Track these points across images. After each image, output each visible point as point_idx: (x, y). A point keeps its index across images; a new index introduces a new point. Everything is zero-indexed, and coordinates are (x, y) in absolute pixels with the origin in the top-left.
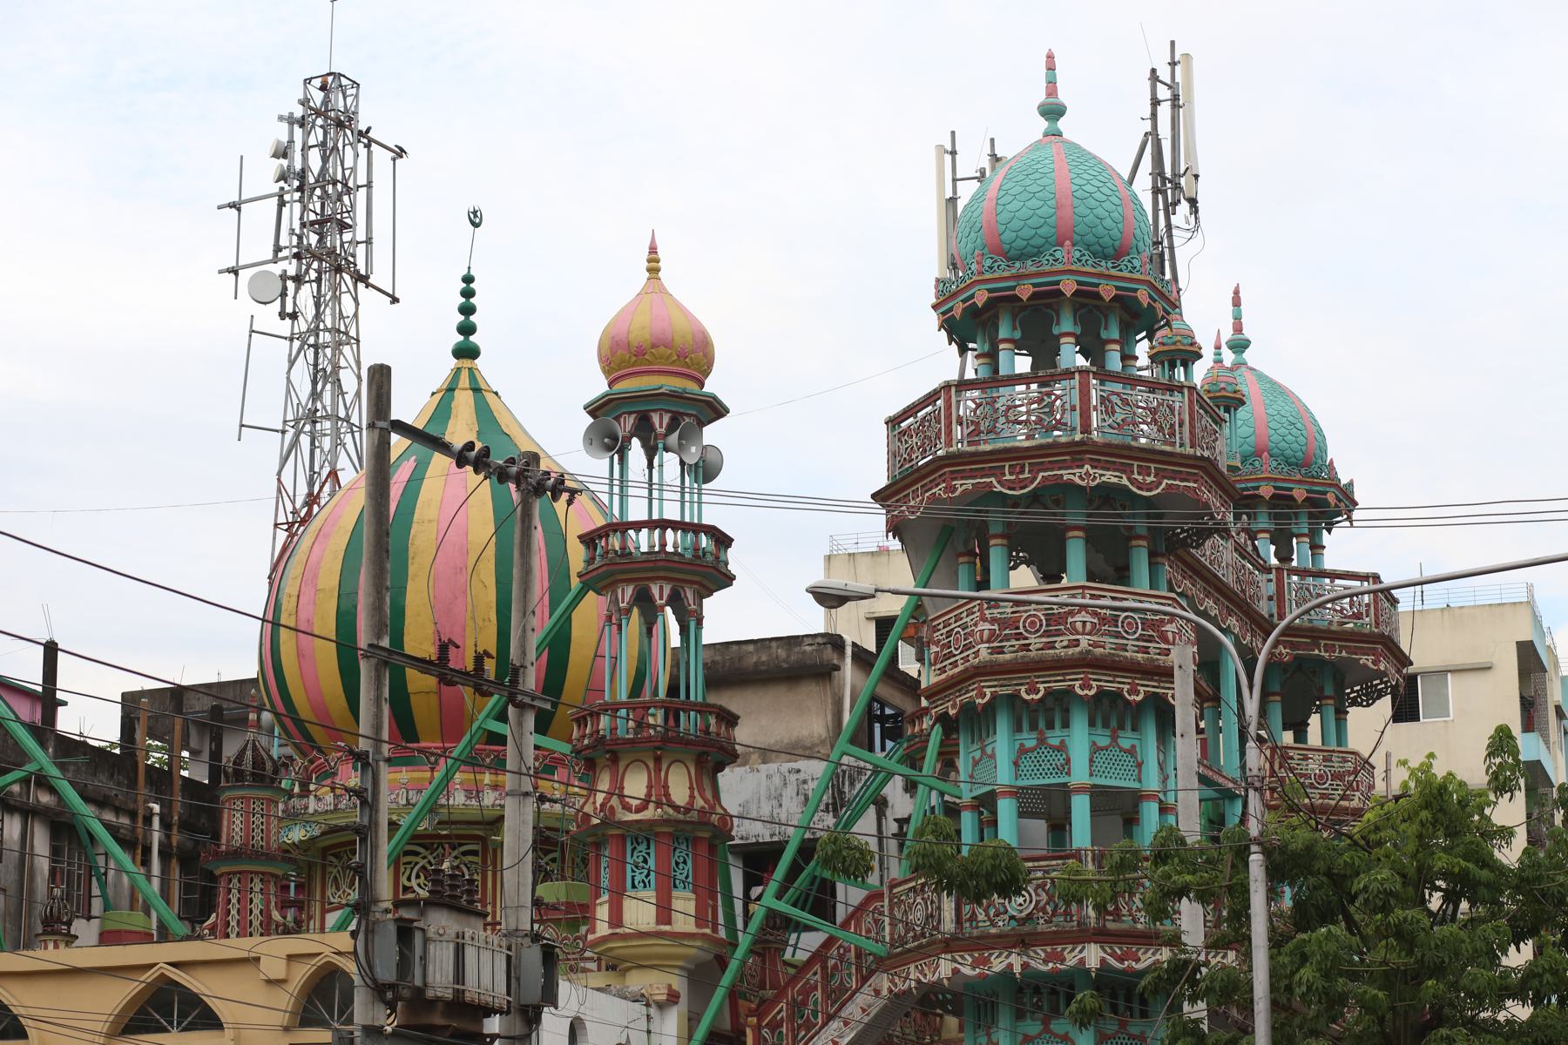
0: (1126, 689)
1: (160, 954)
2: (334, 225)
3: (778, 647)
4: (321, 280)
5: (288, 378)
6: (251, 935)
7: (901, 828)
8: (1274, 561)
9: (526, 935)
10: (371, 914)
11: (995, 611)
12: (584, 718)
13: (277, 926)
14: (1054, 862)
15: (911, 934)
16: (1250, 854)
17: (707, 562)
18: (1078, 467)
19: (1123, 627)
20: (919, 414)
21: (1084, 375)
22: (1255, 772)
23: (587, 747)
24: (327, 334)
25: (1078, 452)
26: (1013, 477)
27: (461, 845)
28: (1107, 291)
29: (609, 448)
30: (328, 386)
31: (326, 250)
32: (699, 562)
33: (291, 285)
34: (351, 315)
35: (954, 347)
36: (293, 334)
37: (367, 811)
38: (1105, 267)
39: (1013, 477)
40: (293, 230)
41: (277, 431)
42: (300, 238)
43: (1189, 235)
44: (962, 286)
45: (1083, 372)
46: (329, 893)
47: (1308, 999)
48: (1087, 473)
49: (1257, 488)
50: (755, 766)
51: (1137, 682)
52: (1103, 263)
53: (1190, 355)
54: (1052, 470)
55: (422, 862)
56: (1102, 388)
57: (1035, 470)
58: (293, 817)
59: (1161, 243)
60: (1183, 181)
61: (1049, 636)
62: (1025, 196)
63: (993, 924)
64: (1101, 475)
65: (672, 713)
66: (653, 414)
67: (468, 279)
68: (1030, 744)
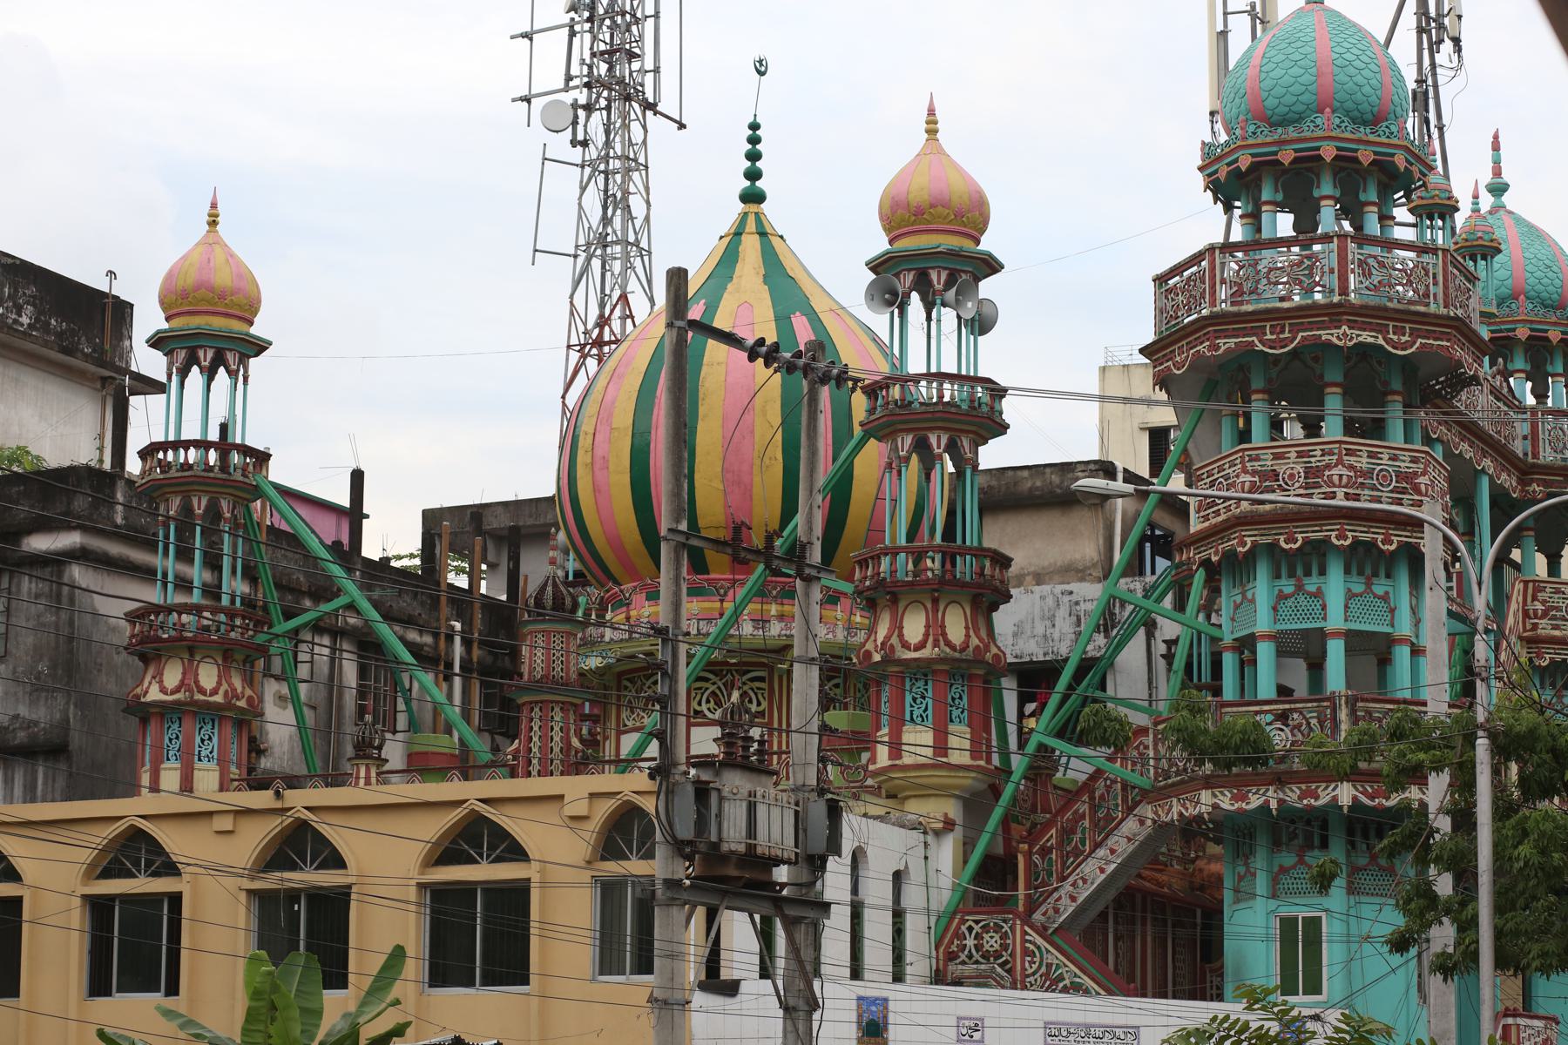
0: (1379, 540)
1: (471, 791)
2: (623, 55)
3: (1052, 473)
4: (611, 107)
5: (580, 204)
6: (552, 775)
7: (1169, 649)
8: (1531, 400)
9: (813, 790)
10: (671, 776)
11: (1256, 464)
12: (866, 560)
13: (577, 752)
14: (1310, 705)
15: (1174, 769)
16: (1476, 738)
17: (983, 413)
18: (1336, 328)
19: (1378, 479)
20: (1185, 274)
21: (1343, 239)
22: (1482, 663)
23: (869, 589)
24: (617, 161)
25: (1335, 313)
26: (1274, 337)
27: (749, 671)
28: (1366, 156)
29: (890, 304)
30: (619, 212)
31: (616, 79)
32: (974, 413)
34: (640, 141)
35: (1220, 205)
36: (584, 161)
37: (667, 682)
38: (1364, 132)
39: (1274, 337)
40: (584, 60)
41: (569, 255)
42: (590, 67)
43: (1453, 73)
44: (1227, 150)
45: (1343, 237)
46: (624, 715)
47: (1525, 873)
48: (1345, 334)
49: (1514, 330)
50: (1030, 588)
51: (1391, 532)
52: (1362, 129)
53: (1446, 209)
54: (1311, 330)
55: (713, 688)
56: (1360, 251)
57: (1295, 330)
58: (589, 644)
59: (1425, 81)
60: (1446, 21)
61: (1306, 489)
62: (1288, 64)
64: (1358, 336)
65: (949, 557)
66: (931, 271)
67: (754, 127)
68: (1289, 590)
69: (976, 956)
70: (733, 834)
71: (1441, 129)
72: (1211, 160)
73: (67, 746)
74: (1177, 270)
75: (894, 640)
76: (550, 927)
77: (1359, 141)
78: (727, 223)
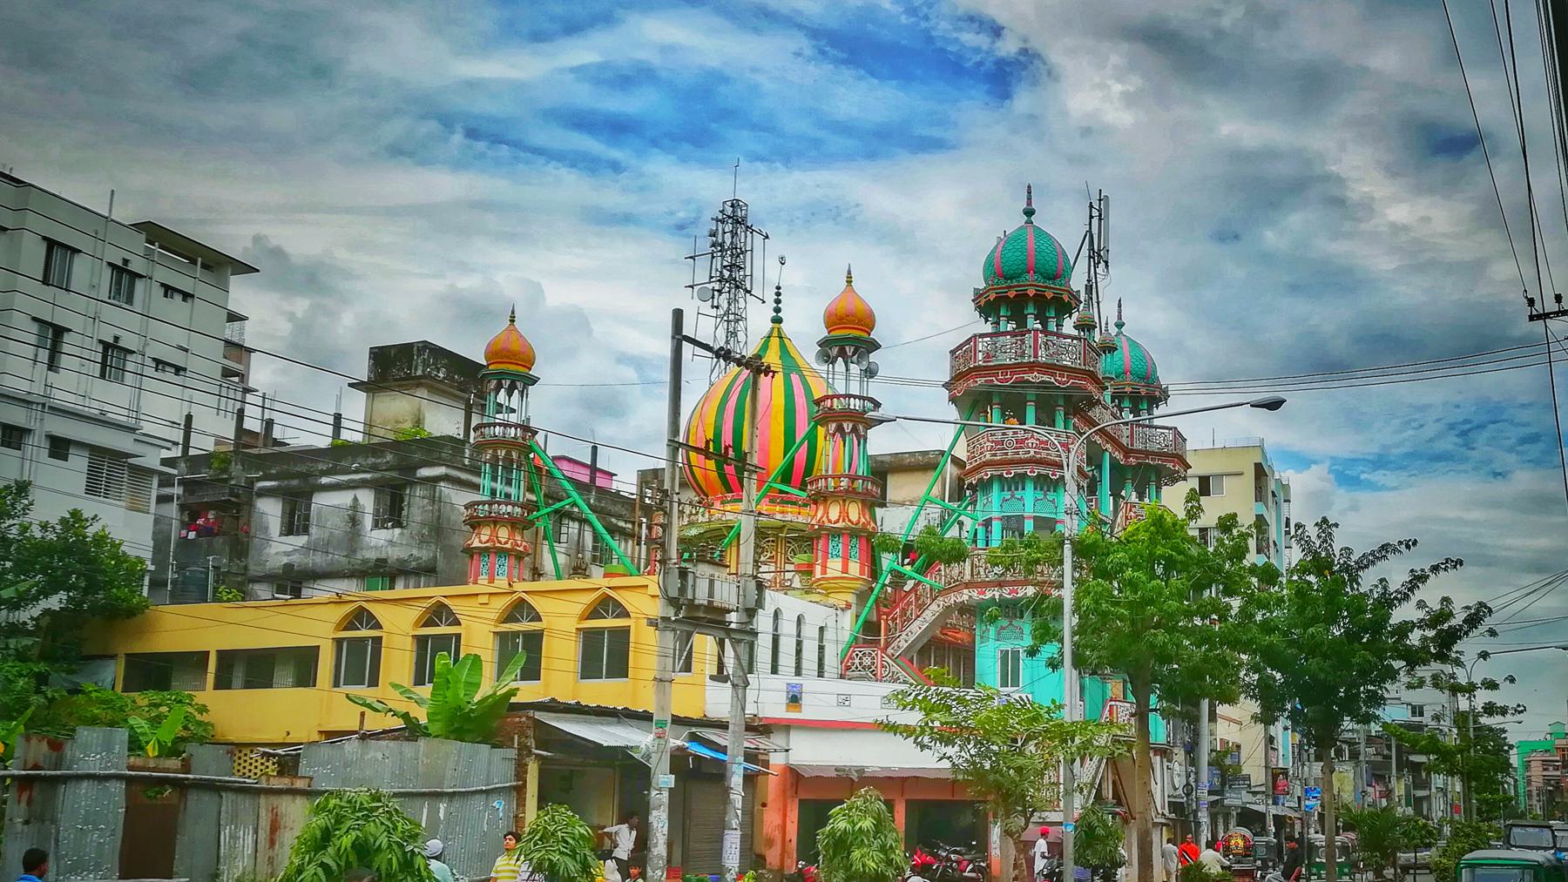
20: (964, 349)
23: (813, 495)
25: (1032, 367)
28: (1049, 295)
29: (827, 362)
33: (716, 293)
38: (1049, 283)
42: (721, 272)
45: (1036, 330)
48: (1036, 376)
60: (1102, 253)
63: (987, 577)
69: (860, 668)
70: (702, 597)
71: (1098, 303)
72: (978, 295)
73: (435, 568)
74: (960, 347)
75: (825, 519)
76: (644, 647)
77: (1046, 287)
78: (766, 332)
